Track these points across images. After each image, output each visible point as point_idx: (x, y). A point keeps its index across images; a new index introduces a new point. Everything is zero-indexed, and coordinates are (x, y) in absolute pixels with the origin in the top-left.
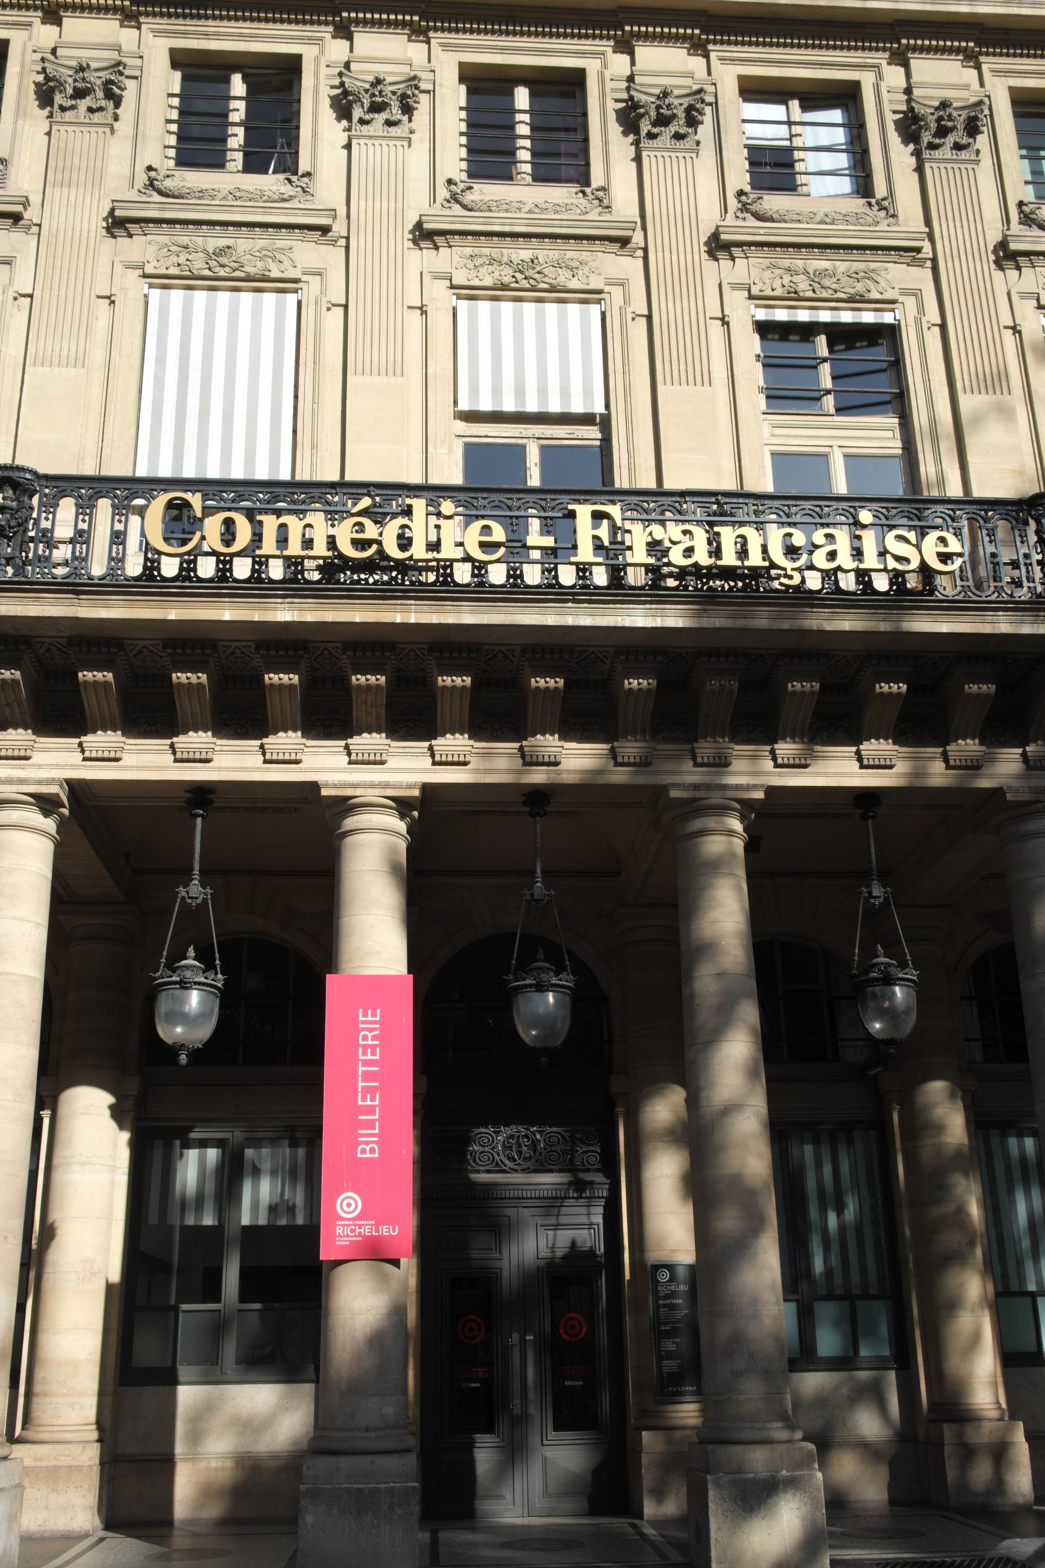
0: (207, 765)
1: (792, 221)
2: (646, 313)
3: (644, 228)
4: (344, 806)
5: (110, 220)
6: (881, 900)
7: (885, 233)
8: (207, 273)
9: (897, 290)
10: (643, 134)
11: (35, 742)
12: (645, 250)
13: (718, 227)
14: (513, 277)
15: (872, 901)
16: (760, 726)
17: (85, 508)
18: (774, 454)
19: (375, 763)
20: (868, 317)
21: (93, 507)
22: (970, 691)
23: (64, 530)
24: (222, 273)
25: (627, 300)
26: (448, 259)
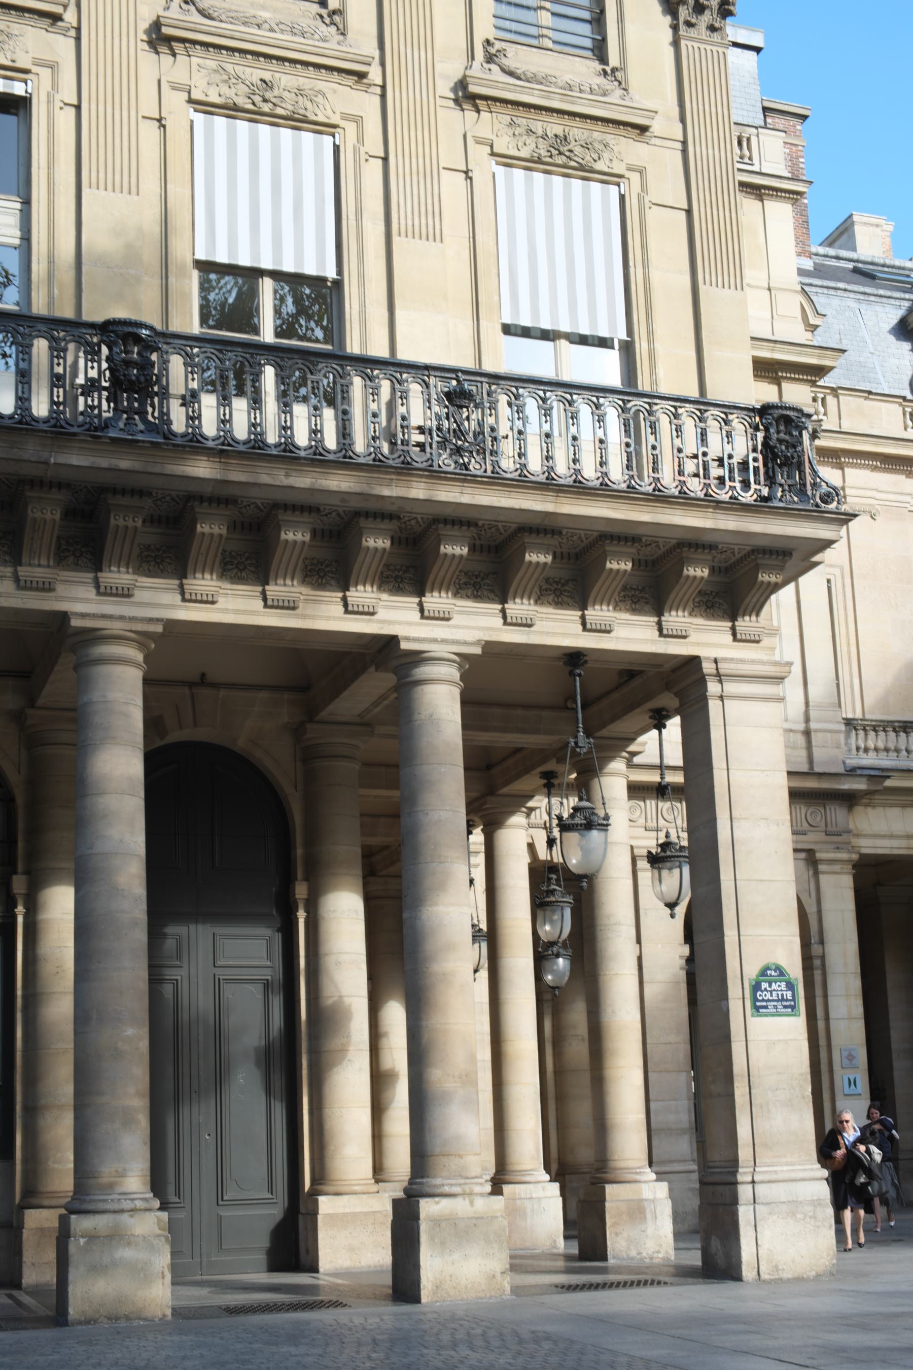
0: (372, 617)
1: (233, 20)
2: (686, 207)
3: (383, 64)
4: (92, 637)
6: (585, 750)
7: (325, 44)
8: (251, 107)
9: (338, 116)
10: (681, 20)
12: (78, 29)
13: (158, 17)
16: (171, 557)
19: (207, 602)
24: (266, 108)
25: (361, 139)
26: (487, 124)
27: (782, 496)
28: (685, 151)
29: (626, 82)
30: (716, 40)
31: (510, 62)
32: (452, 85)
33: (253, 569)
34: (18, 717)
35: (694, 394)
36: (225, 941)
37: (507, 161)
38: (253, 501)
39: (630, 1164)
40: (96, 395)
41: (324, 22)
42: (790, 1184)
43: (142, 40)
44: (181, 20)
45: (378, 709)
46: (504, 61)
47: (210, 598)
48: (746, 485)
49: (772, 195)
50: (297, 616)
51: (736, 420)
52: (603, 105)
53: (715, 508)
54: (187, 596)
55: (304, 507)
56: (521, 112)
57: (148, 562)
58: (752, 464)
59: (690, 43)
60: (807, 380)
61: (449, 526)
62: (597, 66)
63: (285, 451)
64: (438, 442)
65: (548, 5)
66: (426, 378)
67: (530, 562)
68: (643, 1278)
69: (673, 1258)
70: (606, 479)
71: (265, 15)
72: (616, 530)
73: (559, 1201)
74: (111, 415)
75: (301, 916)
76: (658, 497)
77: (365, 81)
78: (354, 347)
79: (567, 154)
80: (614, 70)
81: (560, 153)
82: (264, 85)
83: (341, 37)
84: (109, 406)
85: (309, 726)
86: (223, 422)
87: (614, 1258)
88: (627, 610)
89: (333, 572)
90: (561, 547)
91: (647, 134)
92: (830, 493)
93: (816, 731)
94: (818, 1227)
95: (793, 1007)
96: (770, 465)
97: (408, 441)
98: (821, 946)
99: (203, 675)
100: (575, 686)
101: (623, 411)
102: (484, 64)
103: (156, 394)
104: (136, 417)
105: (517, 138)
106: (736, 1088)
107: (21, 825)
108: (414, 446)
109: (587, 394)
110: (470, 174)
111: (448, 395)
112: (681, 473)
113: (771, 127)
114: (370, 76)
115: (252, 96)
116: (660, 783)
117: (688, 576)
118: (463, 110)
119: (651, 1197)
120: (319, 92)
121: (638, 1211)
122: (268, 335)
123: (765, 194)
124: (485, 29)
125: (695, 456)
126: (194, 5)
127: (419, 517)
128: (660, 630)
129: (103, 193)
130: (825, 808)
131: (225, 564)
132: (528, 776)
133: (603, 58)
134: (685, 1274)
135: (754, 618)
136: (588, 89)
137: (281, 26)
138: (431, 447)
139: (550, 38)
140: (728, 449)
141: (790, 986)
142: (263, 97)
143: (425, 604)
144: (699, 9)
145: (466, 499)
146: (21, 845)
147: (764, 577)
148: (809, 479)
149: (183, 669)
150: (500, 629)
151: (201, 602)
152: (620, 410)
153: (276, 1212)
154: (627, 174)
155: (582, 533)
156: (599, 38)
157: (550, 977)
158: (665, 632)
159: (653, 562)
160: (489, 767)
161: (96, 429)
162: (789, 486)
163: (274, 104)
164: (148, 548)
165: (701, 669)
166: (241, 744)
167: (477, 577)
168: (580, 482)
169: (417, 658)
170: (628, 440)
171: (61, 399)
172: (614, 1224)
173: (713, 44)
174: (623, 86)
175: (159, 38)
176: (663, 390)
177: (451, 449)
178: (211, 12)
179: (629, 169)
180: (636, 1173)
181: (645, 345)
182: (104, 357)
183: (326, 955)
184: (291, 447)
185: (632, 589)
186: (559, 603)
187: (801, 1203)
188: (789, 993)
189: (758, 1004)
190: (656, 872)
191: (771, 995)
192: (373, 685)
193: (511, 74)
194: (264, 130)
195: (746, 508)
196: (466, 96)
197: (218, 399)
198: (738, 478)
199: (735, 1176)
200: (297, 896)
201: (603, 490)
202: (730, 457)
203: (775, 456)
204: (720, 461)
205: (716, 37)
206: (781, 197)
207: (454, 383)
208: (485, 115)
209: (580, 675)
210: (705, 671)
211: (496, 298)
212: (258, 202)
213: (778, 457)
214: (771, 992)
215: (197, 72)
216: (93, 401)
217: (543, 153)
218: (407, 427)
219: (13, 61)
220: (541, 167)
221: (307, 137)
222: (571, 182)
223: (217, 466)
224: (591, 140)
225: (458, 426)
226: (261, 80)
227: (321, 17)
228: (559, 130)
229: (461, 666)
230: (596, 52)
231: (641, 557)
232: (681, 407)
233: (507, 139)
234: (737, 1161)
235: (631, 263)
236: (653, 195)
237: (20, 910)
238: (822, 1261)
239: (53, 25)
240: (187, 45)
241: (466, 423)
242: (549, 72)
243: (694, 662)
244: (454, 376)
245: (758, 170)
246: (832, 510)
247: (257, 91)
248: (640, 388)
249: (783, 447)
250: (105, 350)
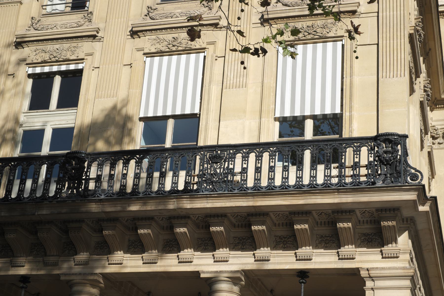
1: (161, 18)
5: (262, 20)
8: (168, 50)
11: (356, 251)
17: (245, 158)
19: (394, 257)
20: (72, 67)
21: (360, 151)
22: (213, 230)
23: (238, 169)
24: (174, 49)
40: (358, 169)
50: (157, 266)
77: (219, 26)
81: (309, 34)
88: (365, 247)
89: (291, 241)
115: (168, 46)
162: (390, 174)
167: (244, 239)
184: (259, 188)
185: (326, 236)
193: (286, 5)
215: (146, 42)
220: (301, 42)
224: (326, 24)
226: (173, 38)
243: (356, 272)
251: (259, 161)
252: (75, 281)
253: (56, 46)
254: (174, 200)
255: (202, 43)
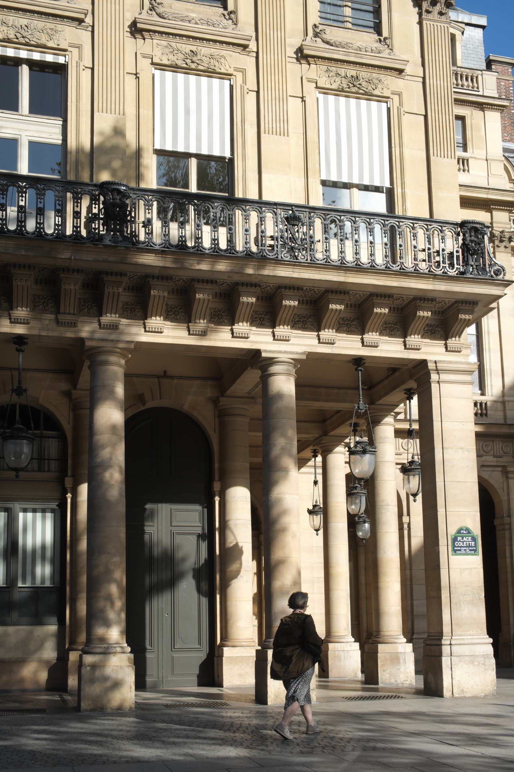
1: (175, 19)
3: (257, 40)
6: (363, 411)
7: (226, 30)
8: (185, 66)
9: (232, 69)
12: (93, 27)
13: (135, 18)
14: (15, 35)
15: (360, 411)
18: (29, 142)
19: (158, 332)
20: (49, 58)
24: (193, 66)
25: (244, 81)
26: (314, 71)
27: (472, 271)
28: (424, 83)
29: (392, 45)
30: (443, 20)
31: (327, 37)
32: (295, 50)
33: (183, 314)
34: (68, 394)
35: (427, 216)
36: (177, 513)
37: (325, 91)
38: (181, 278)
39: (392, 633)
40: (97, 222)
41: (225, 18)
42: (471, 646)
43: (127, 31)
44: (148, 19)
45: (257, 390)
46: (324, 36)
47: (159, 330)
48: (452, 265)
49: (489, 108)
51: (447, 230)
52: (378, 58)
53: (274, 263)
54: (147, 329)
55: (209, 280)
56: (333, 64)
57: (127, 311)
58: (455, 254)
59: (428, 22)
60: (506, 210)
61: (287, 290)
62: (376, 37)
63: (198, 250)
64: (281, 245)
65: (349, 4)
66: (275, 210)
67: (332, 309)
68: (395, 694)
69: (414, 684)
70: (374, 263)
71: (193, 15)
72: (380, 291)
73: (359, 653)
74: (105, 232)
75: (217, 499)
76: (403, 273)
77: (247, 49)
78: (239, 194)
79: (358, 86)
80: (385, 39)
81: (354, 86)
82: (192, 54)
83: (235, 26)
84: (104, 228)
85: (221, 399)
86: (341, 252)
87: (382, 683)
88: (428, 338)
89: (226, 316)
90: (350, 301)
91: (403, 74)
92: (499, 269)
93: (508, 401)
94: (486, 669)
95: (475, 551)
96: (466, 254)
97: (265, 244)
98: (509, 518)
99: (165, 372)
100: (359, 376)
101: (384, 226)
102: (313, 38)
103: (129, 221)
104: (118, 234)
105: (331, 78)
106: (442, 594)
107: (70, 451)
108: (268, 247)
109: (364, 217)
110: (304, 99)
111: (287, 219)
112: (415, 259)
113: (494, 70)
114: (250, 47)
115: (185, 60)
116: (409, 429)
117: (420, 316)
118: (301, 64)
119: (403, 651)
120: (222, 56)
121: (395, 659)
122: (193, 188)
123: (485, 107)
124: (314, 18)
125: (424, 250)
126: (155, 11)
127: (271, 285)
128: (405, 345)
129: (105, 114)
130: (493, 442)
131: (168, 311)
132: (343, 425)
133: (380, 33)
134: (418, 693)
135: (457, 339)
136: (370, 50)
137: (201, 21)
138: (277, 248)
139: (350, 23)
140: (442, 246)
141: (474, 539)
142: (191, 60)
143: (275, 333)
144: (434, 2)
145: (295, 275)
146: (70, 462)
147: (462, 316)
148: (487, 262)
149: (153, 368)
150: (317, 346)
151: (155, 332)
152: (382, 226)
153: (202, 655)
154: (391, 96)
155: (361, 292)
156: (378, 21)
157: (360, 534)
158: (408, 346)
159: (402, 308)
160: (324, 421)
161: (97, 241)
162: (476, 266)
163: (198, 64)
164: (127, 303)
165: (428, 366)
166: (186, 408)
168: (359, 265)
169: (271, 361)
170: (429, 246)
171: (60, 223)
172: (382, 666)
173: (441, 22)
174: (390, 47)
175: (135, 30)
176: (410, 214)
177: (288, 248)
178: (164, 14)
179: (392, 94)
180: (395, 638)
181: (400, 190)
182: (101, 202)
183: (229, 520)
184: (201, 248)
185: (390, 323)
186: (349, 332)
187: (477, 656)
188: (473, 543)
189: (456, 548)
190: (406, 477)
191: (463, 544)
192: (252, 376)
193: (328, 43)
194: (192, 78)
195: (451, 278)
196: (302, 56)
197: (162, 223)
198: (447, 262)
199: (441, 641)
200: (215, 489)
201: (372, 269)
202: (443, 250)
203: (468, 250)
204: (438, 252)
205: (443, 18)
206: (494, 109)
207: (291, 212)
208: (313, 66)
209: (361, 370)
210: (429, 368)
211: (318, 166)
212: (184, 117)
213: (470, 250)
214: (463, 542)
215: (156, 48)
216: (95, 225)
217: (345, 86)
218: (264, 236)
219: (58, 45)
220: (344, 93)
221: (216, 82)
222: (339, 99)
223: (160, 259)
224: (371, 78)
225: (292, 235)
226: (191, 51)
227: (224, 15)
228: (353, 73)
229: (295, 366)
230: (376, 29)
231: (395, 306)
232: (417, 223)
233: (325, 79)
234: (442, 633)
235: (393, 145)
236: (406, 107)
237: (69, 495)
238: (488, 688)
239: (79, 24)
240: (151, 33)
241: (297, 234)
242: (349, 41)
243: (424, 363)
244: (290, 208)
245: (482, 94)
246: (498, 278)
247: (189, 57)
248: (397, 213)
249: (473, 245)
250: (102, 198)
251: (77, 204)
252: (106, 349)
253: (23, 21)
254: (255, 263)
255: (228, 67)
